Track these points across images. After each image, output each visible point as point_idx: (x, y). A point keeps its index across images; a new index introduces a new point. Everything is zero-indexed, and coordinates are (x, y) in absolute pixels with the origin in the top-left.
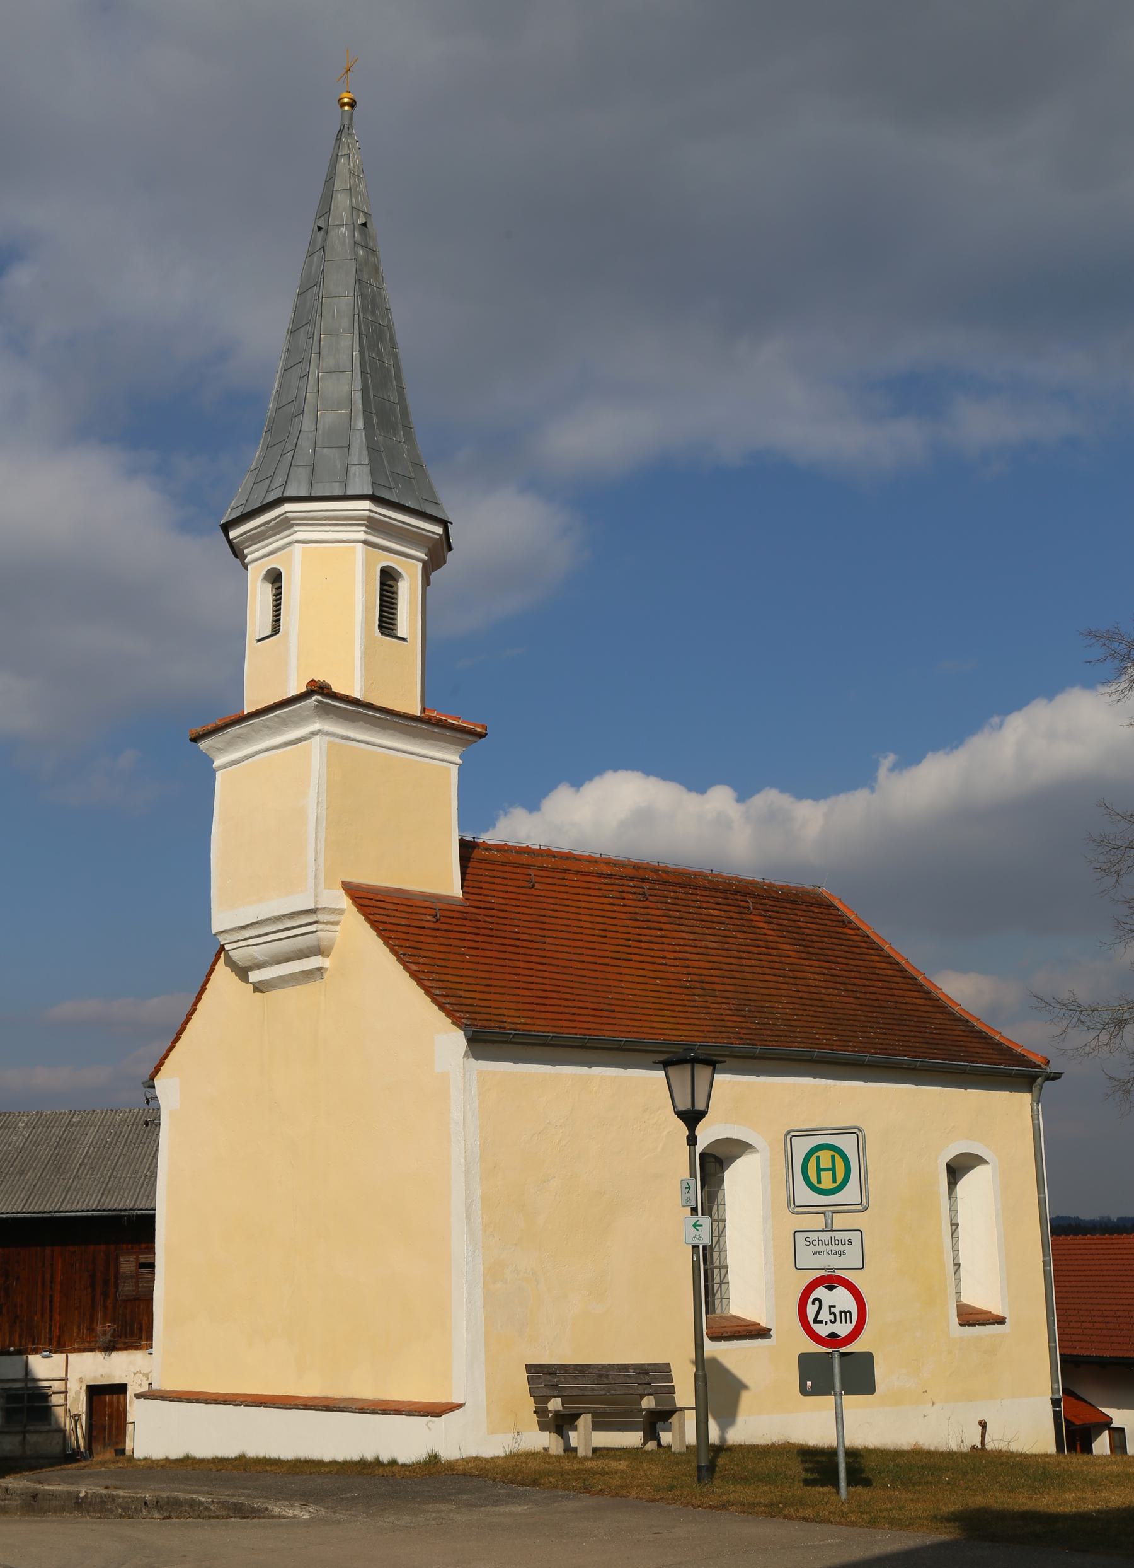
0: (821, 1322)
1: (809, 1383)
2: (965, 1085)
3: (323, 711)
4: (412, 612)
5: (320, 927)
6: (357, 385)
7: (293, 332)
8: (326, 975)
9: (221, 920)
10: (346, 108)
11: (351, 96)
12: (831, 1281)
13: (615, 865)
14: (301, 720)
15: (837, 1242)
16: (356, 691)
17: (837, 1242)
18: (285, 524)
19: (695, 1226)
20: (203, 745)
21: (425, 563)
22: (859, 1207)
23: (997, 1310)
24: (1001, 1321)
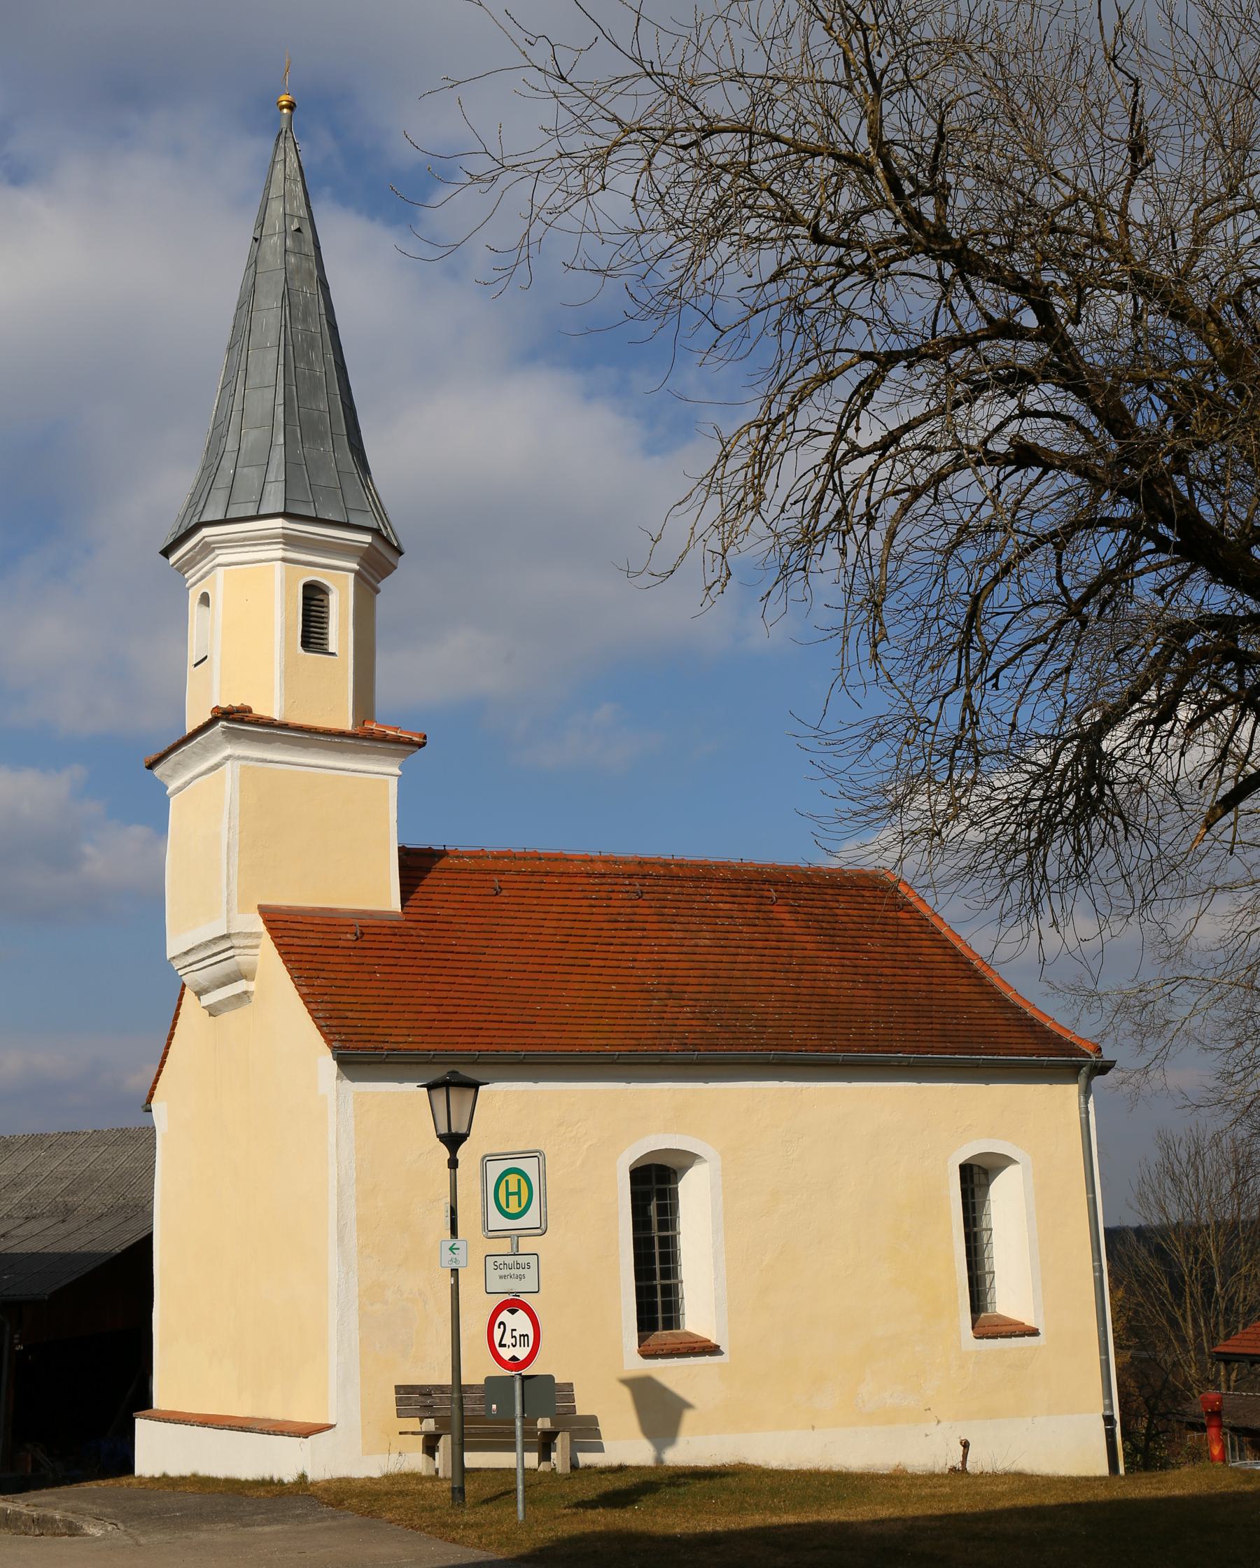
0: (504, 1346)
1: (494, 1407)
2: (988, 1080)
3: (231, 735)
4: (342, 625)
5: (237, 951)
6: (280, 400)
7: (230, 348)
8: (253, 998)
9: (174, 946)
10: (285, 111)
11: (290, 98)
12: (513, 1305)
13: (615, 862)
14: (207, 750)
15: (518, 1266)
16: (276, 715)
17: (518, 1266)
18: (207, 549)
19: (451, 1249)
20: (158, 771)
21: (357, 573)
22: (539, 1231)
23: (1030, 1322)
24: (1034, 1333)
